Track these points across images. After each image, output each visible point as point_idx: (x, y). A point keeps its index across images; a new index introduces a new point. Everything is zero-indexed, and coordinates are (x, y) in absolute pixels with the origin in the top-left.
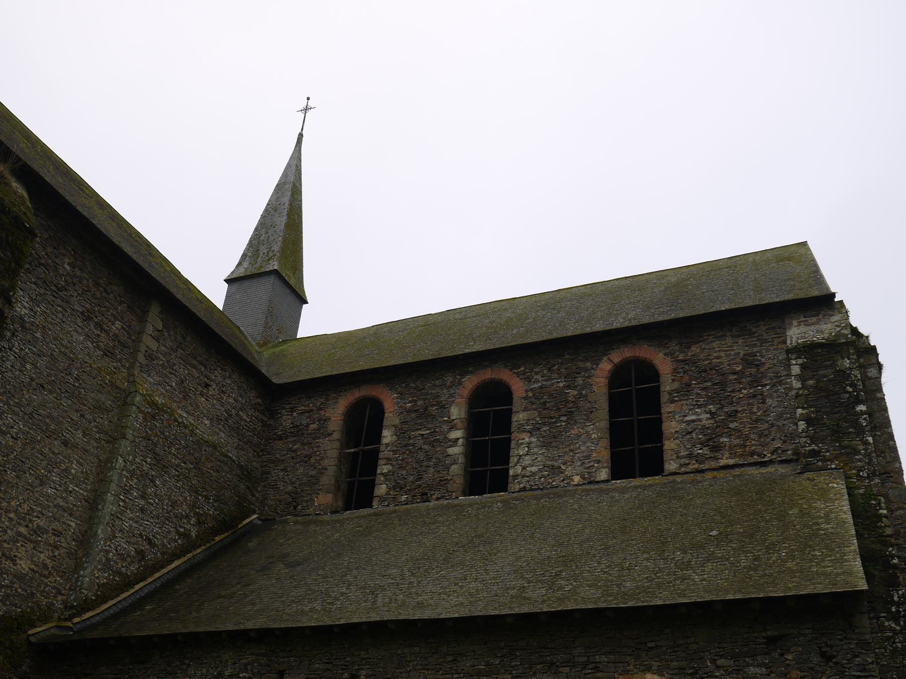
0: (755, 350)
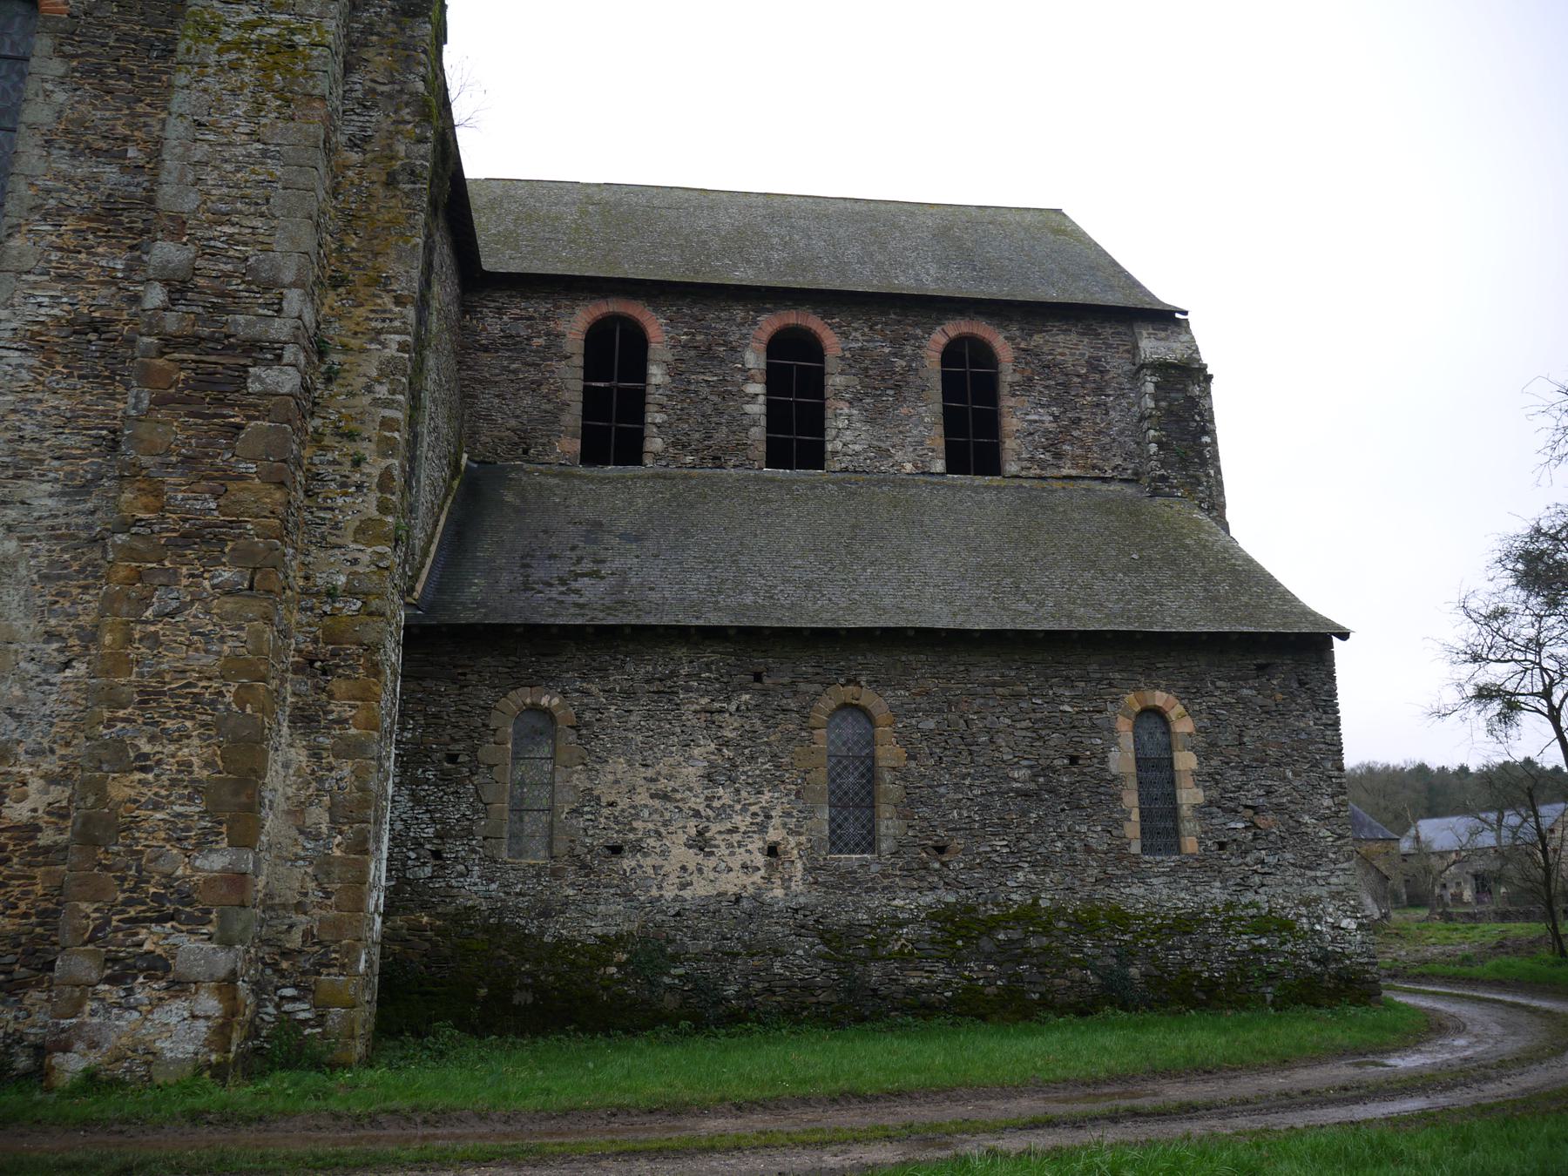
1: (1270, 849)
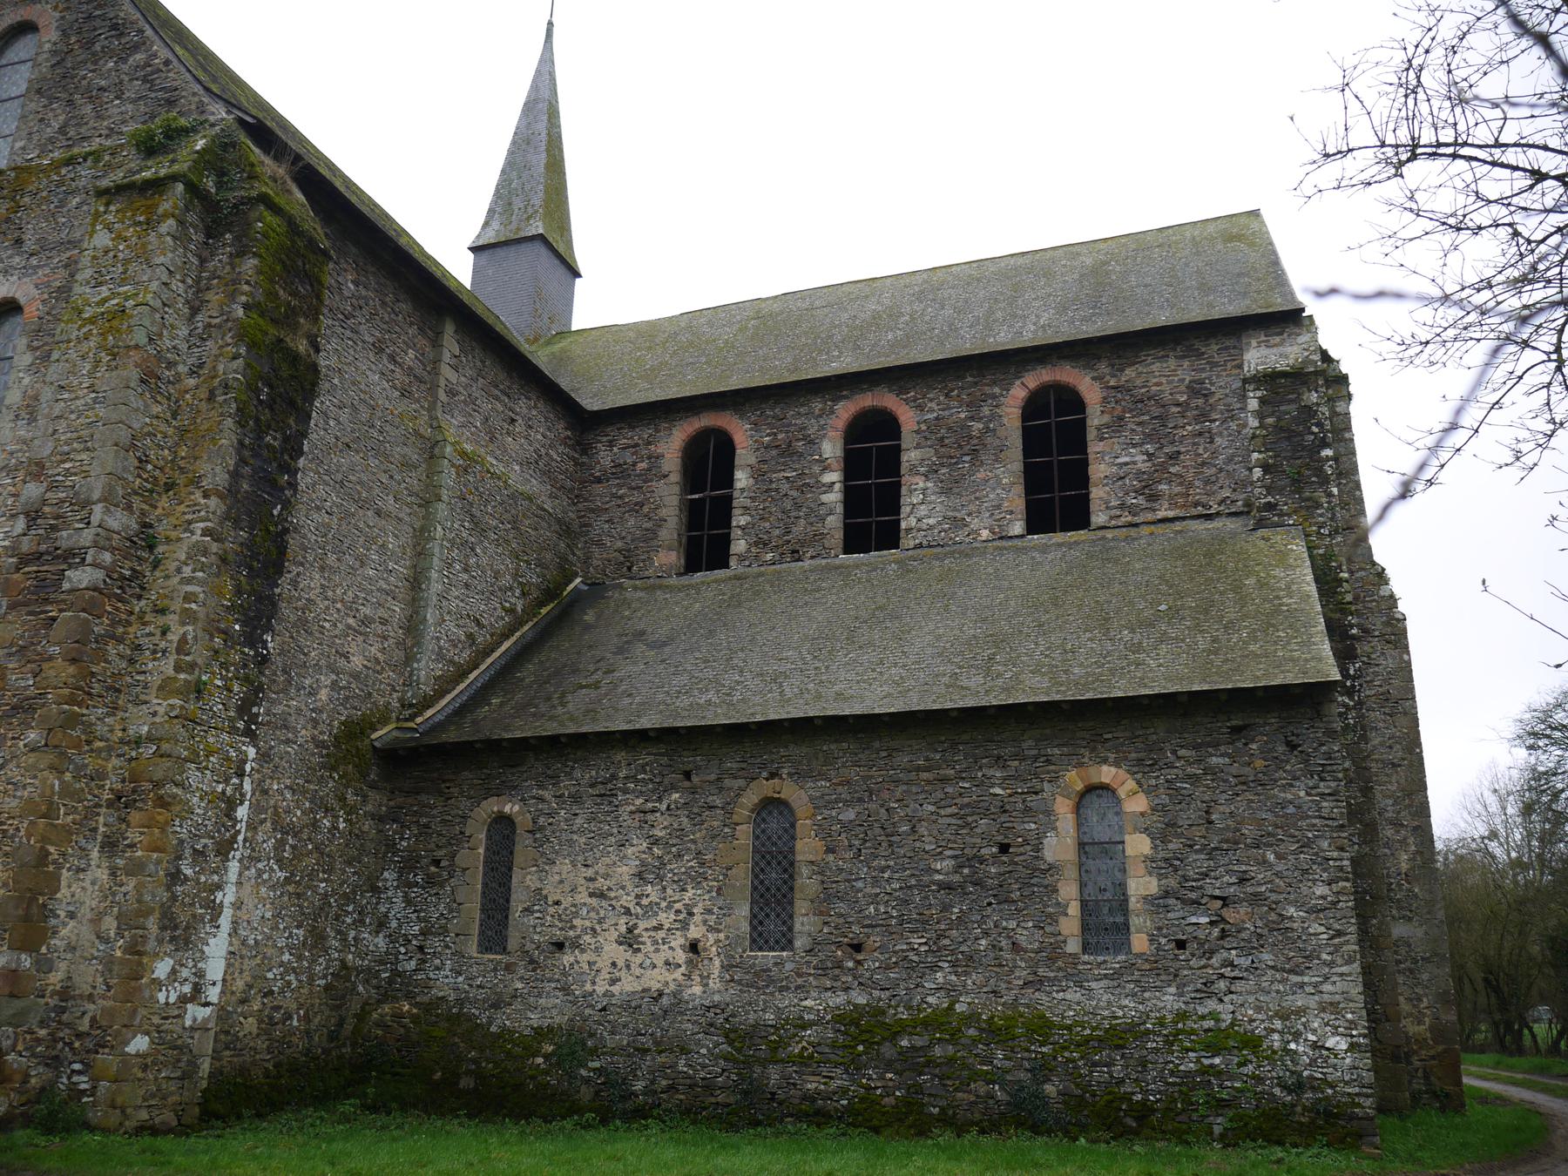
0: (1204, 375)
1: (1242, 948)
